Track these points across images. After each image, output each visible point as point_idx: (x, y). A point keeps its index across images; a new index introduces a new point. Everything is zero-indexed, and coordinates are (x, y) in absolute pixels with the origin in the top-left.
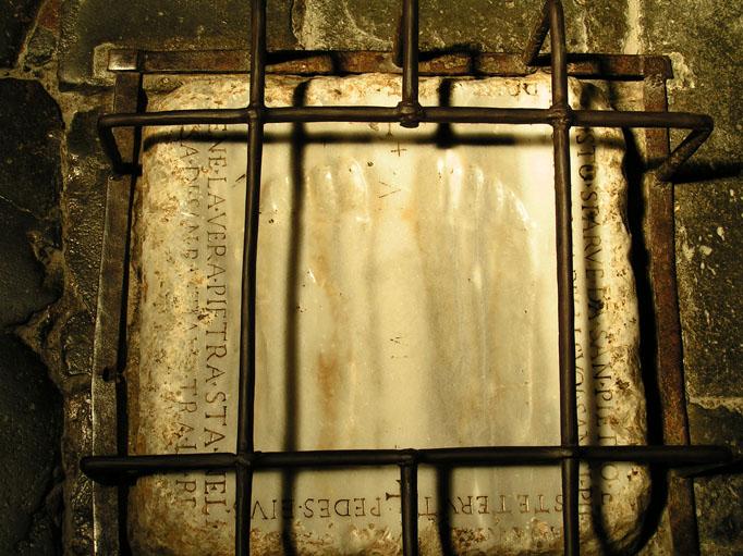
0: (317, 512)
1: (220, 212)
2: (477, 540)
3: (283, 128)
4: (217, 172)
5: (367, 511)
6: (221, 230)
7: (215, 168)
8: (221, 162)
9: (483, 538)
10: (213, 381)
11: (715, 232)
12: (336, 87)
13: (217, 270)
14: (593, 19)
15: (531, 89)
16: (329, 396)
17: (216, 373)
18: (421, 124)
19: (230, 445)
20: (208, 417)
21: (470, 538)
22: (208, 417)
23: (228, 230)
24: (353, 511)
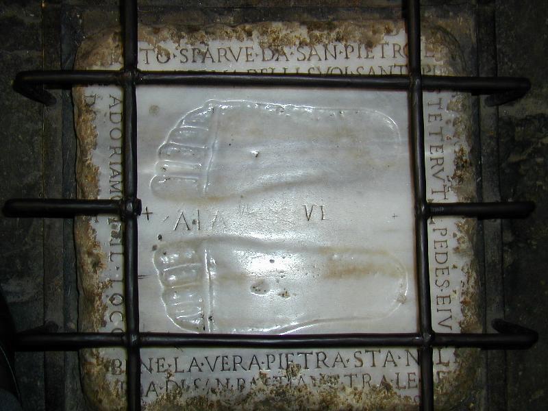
0: (445, 277)
1: (205, 362)
2: (462, 154)
3: (508, 32)
4: (169, 366)
5: (443, 239)
6: (220, 360)
7: (166, 367)
8: (161, 362)
9: (462, 150)
10: (345, 360)
11: (538, 164)
12: (90, 267)
13: (255, 361)
14: (8, 45)
15: (89, 101)
16: (354, 270)
17: (339, 359)
18: (138, 197)
19: (428, 97)
20: (374, 365)
21: (462, 159)
22: (374, 365)
23: (221, 355)
24: (444, 250)
